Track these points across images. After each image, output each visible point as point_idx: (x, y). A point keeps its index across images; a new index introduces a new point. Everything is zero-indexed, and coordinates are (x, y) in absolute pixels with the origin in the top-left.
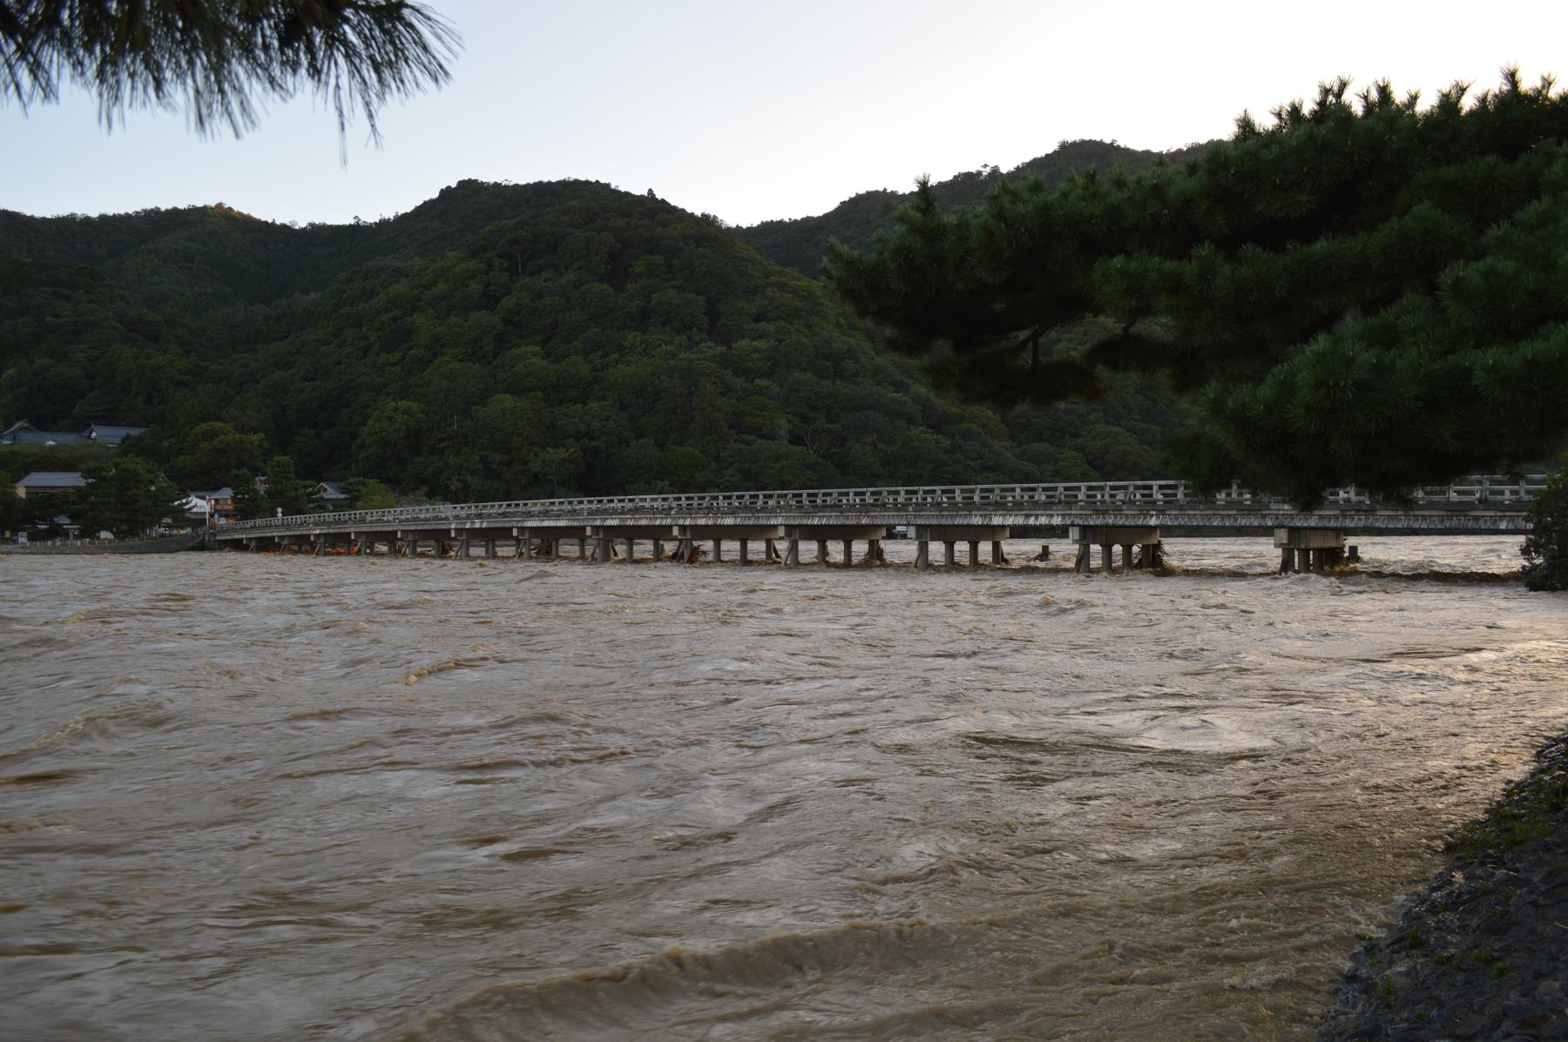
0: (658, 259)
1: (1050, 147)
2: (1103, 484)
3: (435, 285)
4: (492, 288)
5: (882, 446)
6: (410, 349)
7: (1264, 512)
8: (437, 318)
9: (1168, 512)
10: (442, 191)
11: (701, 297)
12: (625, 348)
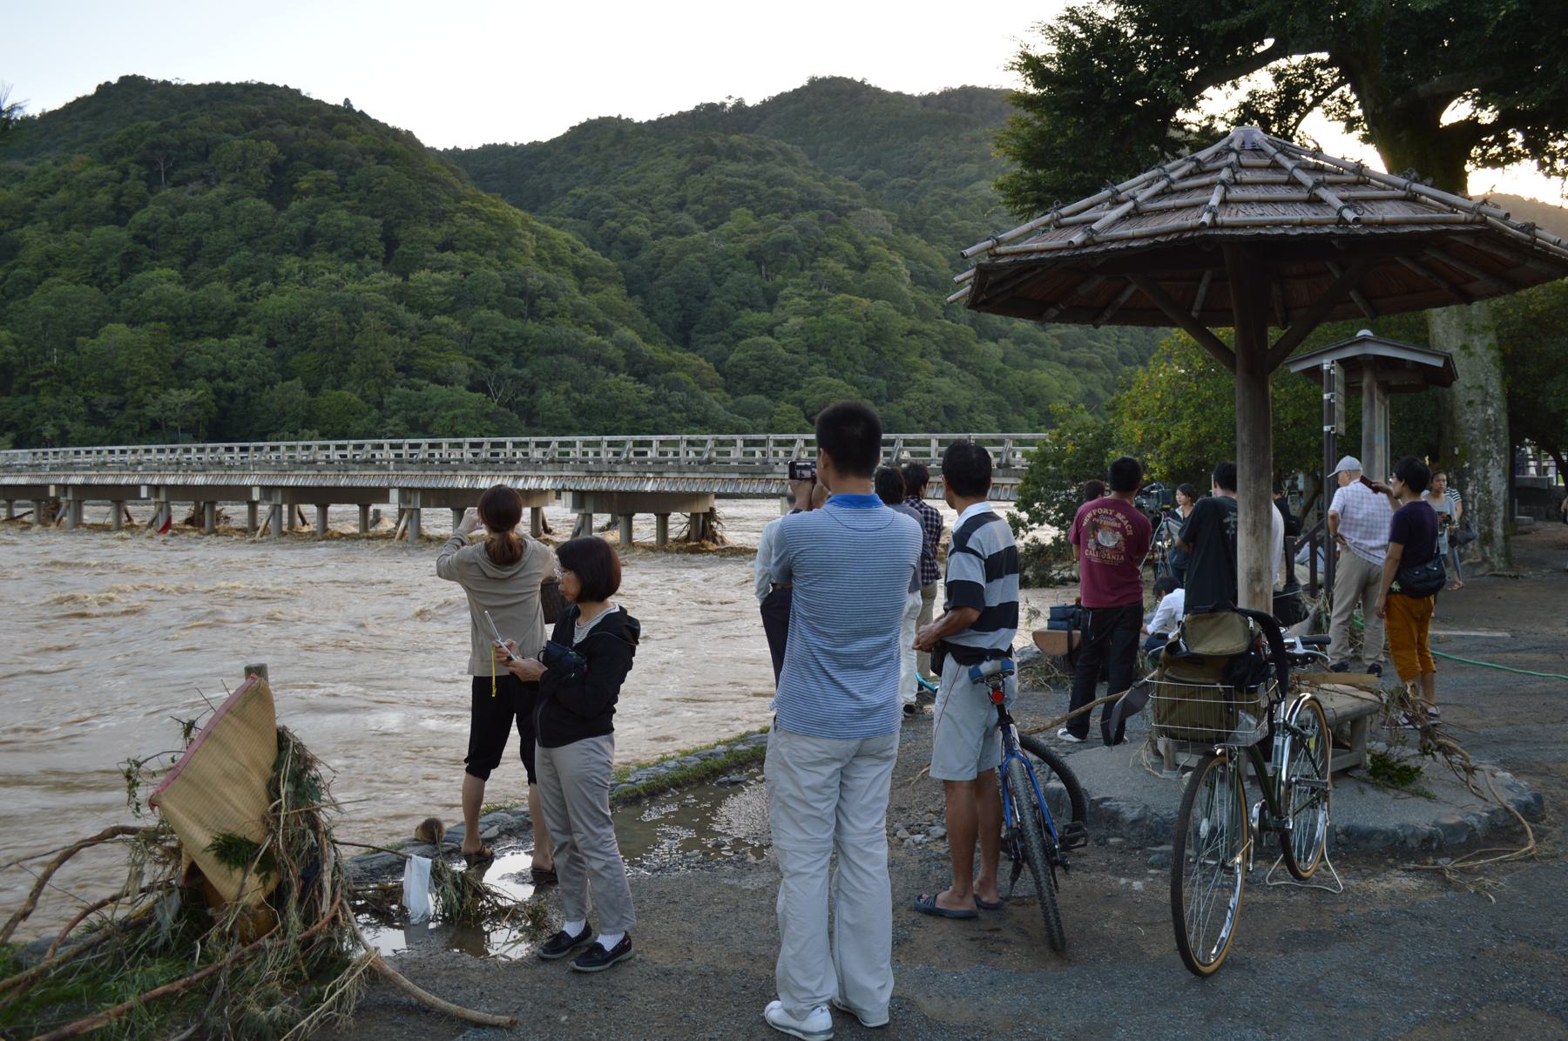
0: (329, 174)
1: (800, 82)
2: (599, 438)
3: (53, 192)
4: (125, 198)
5: (576, 395)
6: (15, 267)
7: (768, 476)
8: (52, 231)
9: (666, 475)
10: (100, 87)
11: (376, 221)
12: (281, 276)
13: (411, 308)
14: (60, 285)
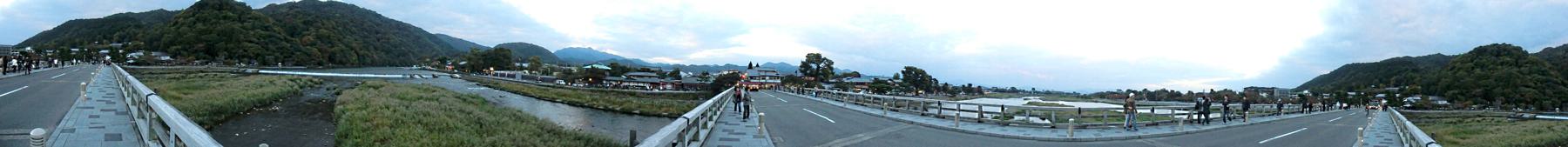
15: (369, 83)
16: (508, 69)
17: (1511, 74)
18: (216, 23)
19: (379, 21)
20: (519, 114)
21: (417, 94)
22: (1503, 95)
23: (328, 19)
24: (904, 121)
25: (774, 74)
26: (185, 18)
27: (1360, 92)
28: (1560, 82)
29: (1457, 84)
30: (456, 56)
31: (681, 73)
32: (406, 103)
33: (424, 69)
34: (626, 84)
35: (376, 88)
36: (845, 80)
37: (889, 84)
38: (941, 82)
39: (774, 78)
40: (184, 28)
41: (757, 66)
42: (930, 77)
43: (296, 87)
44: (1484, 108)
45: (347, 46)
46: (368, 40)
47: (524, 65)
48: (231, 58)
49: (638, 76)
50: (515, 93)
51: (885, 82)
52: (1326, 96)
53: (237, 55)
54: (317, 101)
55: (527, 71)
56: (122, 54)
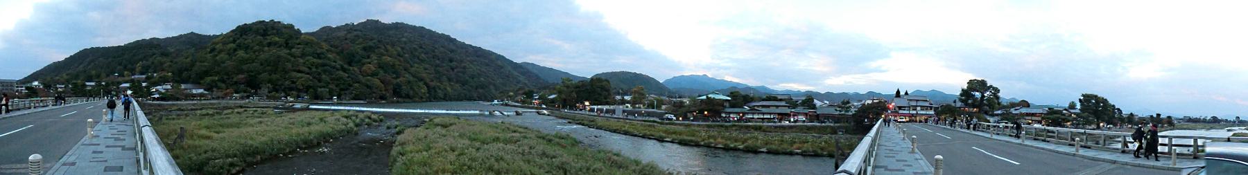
13: (292, 56)
14: (222, 55)
15: (437, 120)
16: (607, 103)
17: (279, 57)
18: (259, 51)
19: (452, 47)
20: (615, 158)
21: (492, 134)
22: (270, 81)
23: (393, 45)
24: (1104, 160)
25: (927, 104)
26: (224, 44)
27: (100, 82)
28: (338, 66)
29: (217, 69)
30: (545, 88)
31: (815, 101)
32: (477, 144)
33: (507, 105)
34: (750, 116)
35: (444, 126)
36: (1013, 111)
37: (1064, 115)
38: (1125, 112)
39: (926, 108)
40: (223, 56)
41: (906, 93)
42: (1114, 106)
43: (351, 125)
44: (248, 97)
45: (414, 76)
46: (441, 69)
47: (626, 98)
48: (277, 91)
49: (763, 106)
50: (615, 131)
51: (1059, 112)
52: (61, 88)
53: (283, 87)
54: (373, 141)
55: (629, 105)
56: (145, 87)
